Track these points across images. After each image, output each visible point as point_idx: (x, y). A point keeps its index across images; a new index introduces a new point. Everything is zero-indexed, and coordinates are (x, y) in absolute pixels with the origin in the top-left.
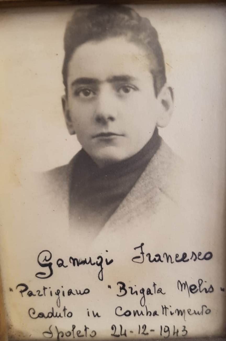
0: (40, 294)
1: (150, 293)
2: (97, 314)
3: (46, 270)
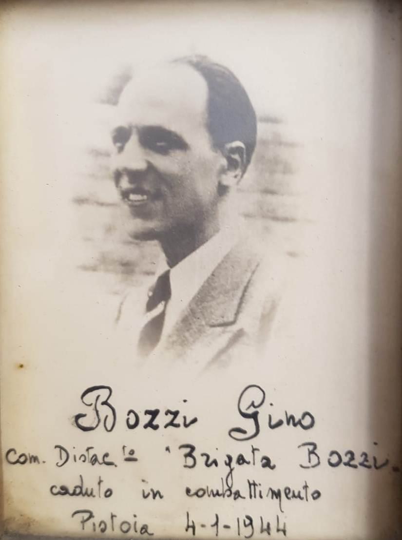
1: (244, 461)
3: (248, 425)
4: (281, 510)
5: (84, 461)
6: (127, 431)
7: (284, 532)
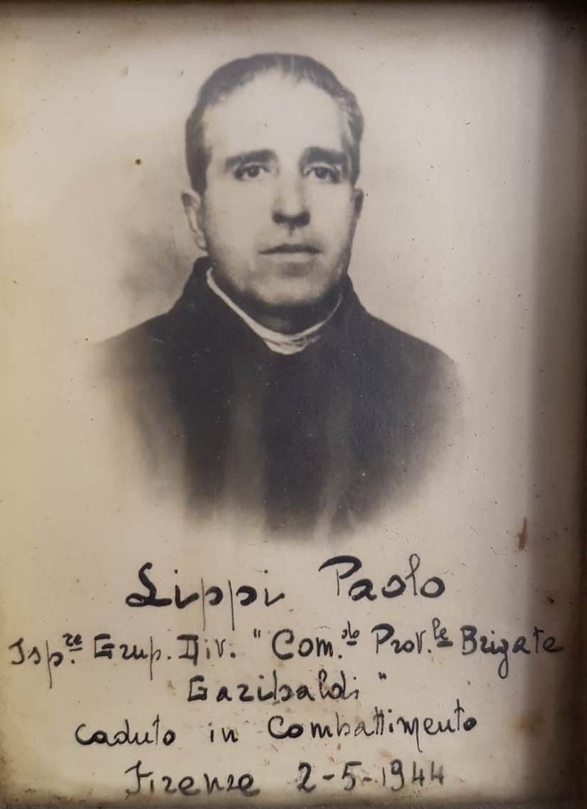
0: (247, 694)
2: (231, 732)
4: (419, 750)
5: (37, 662)
6: (314, 766)
7: (441, 779)
